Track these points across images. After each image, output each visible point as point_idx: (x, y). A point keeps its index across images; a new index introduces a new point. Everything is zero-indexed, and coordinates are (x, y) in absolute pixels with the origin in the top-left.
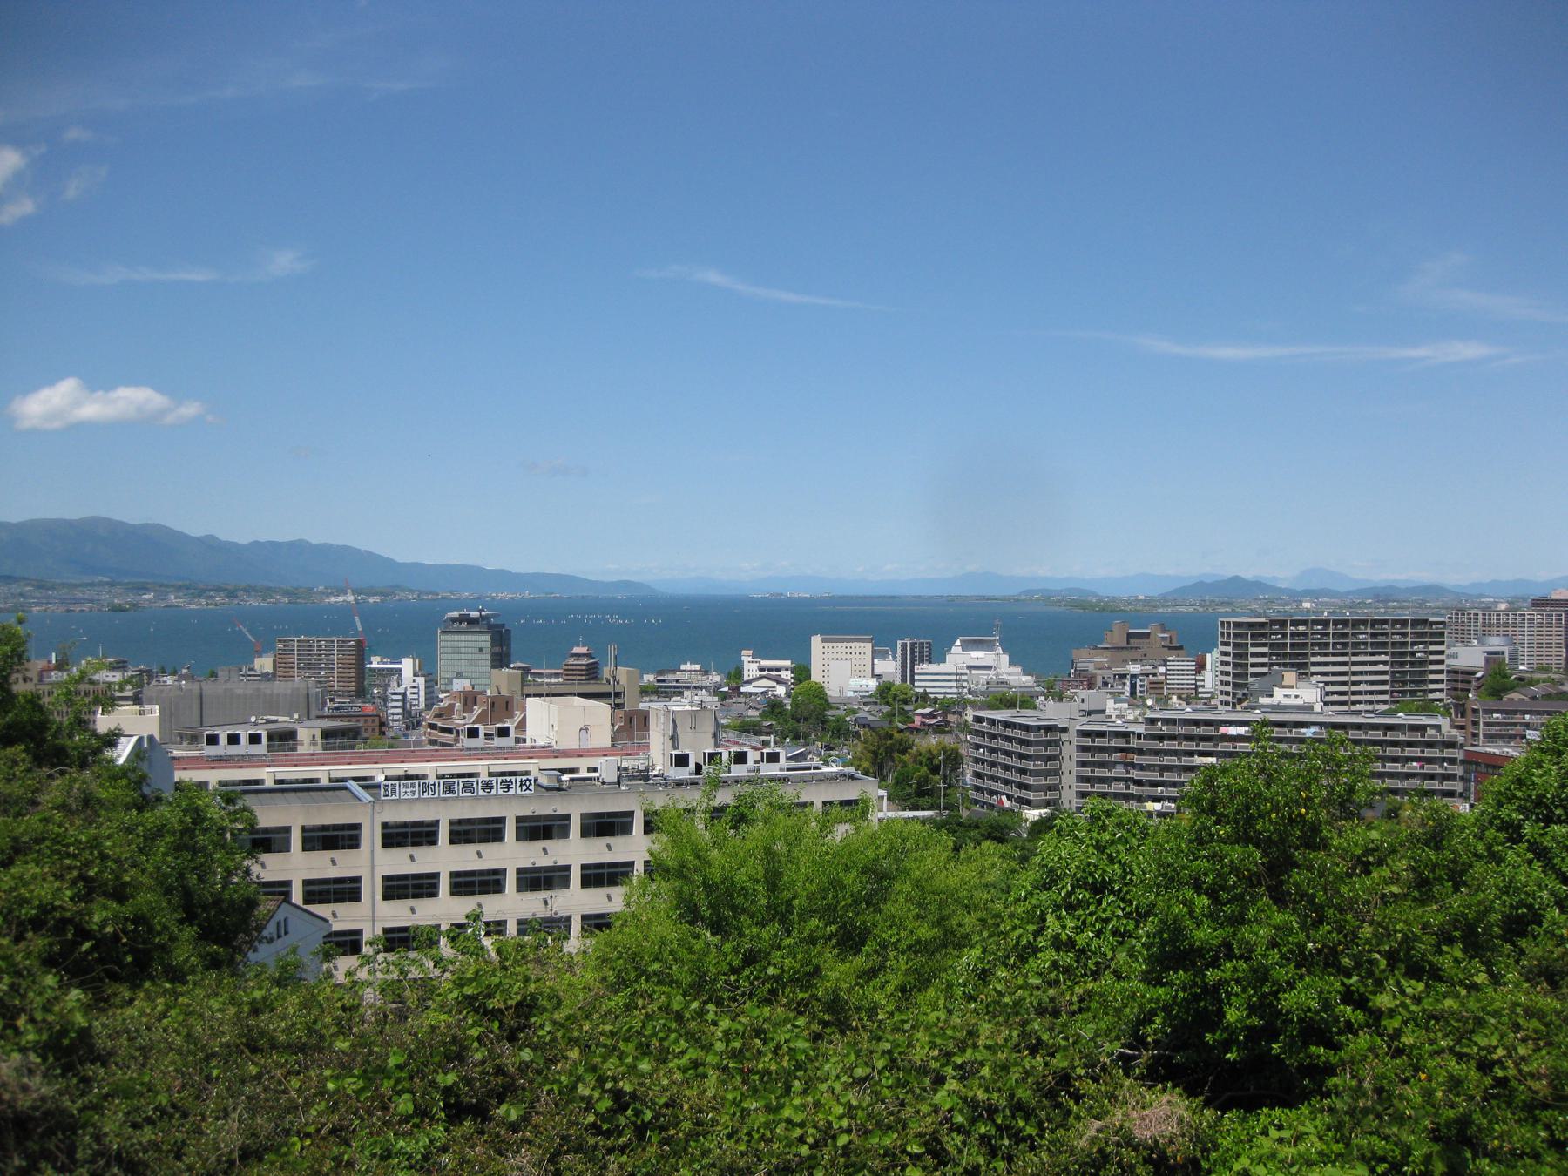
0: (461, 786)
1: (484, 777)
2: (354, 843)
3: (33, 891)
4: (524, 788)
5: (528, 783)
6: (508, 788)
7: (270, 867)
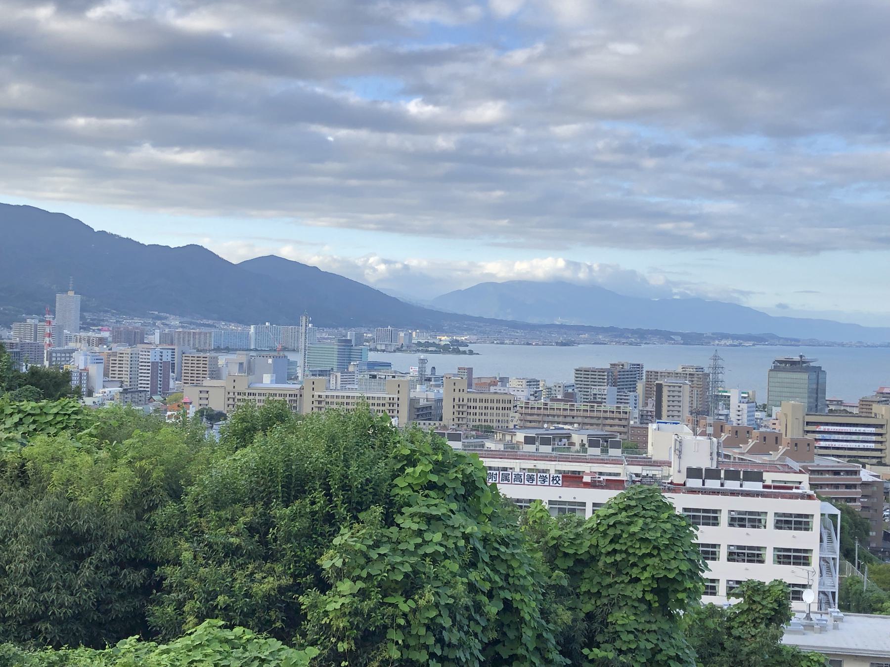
0: (513, 477)
1: (553, 473)
2: (807, 562)
3: (337, 496)
4: (555, 482)
5: (557, 479)
6: (544, 481)
7: (705, 535)
